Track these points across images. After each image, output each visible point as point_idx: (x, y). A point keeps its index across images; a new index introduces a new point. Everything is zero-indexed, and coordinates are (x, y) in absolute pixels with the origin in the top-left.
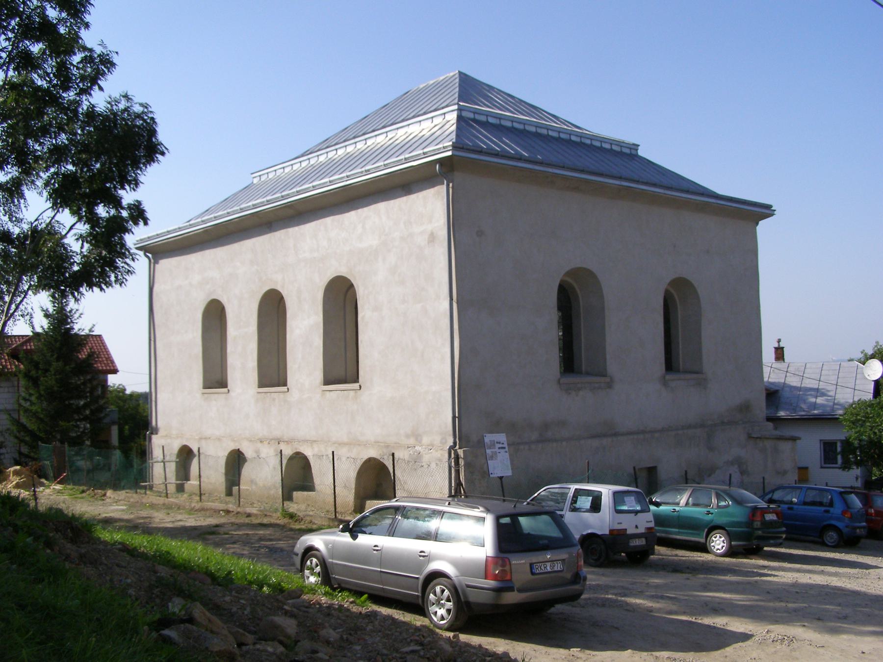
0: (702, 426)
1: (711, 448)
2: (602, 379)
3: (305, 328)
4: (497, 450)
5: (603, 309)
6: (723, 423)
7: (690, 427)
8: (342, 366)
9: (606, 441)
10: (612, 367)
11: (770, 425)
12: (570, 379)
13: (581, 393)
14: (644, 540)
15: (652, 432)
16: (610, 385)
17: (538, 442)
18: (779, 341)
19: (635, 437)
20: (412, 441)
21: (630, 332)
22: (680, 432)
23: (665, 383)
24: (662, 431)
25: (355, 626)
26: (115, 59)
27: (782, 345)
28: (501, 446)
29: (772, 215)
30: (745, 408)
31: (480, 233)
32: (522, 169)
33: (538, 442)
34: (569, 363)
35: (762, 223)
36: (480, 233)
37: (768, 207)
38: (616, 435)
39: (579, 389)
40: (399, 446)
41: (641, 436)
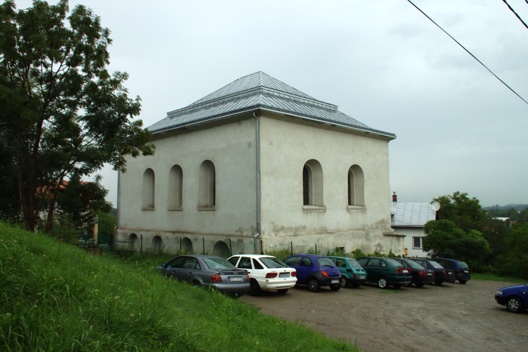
3: (193, 180)
5: (322, 178)
7: (359, 230)
8: (310, 169)
10: (326, 202)
16: (325, 211)
17: (293, 236)
18: (394, 193)
20: (239, 233)
21: (333, 186)
22: (355, 232)
23: (348, 210)
26: (495, 303)
27: (396, 194)
29: (395, 138)
30: (383, 222)
32: (303, 119)
33: (293, 236)
35: (390, 141)
36: (271, 144)
37: (394, 135)
39: (311, 212)
40: (232, 236)
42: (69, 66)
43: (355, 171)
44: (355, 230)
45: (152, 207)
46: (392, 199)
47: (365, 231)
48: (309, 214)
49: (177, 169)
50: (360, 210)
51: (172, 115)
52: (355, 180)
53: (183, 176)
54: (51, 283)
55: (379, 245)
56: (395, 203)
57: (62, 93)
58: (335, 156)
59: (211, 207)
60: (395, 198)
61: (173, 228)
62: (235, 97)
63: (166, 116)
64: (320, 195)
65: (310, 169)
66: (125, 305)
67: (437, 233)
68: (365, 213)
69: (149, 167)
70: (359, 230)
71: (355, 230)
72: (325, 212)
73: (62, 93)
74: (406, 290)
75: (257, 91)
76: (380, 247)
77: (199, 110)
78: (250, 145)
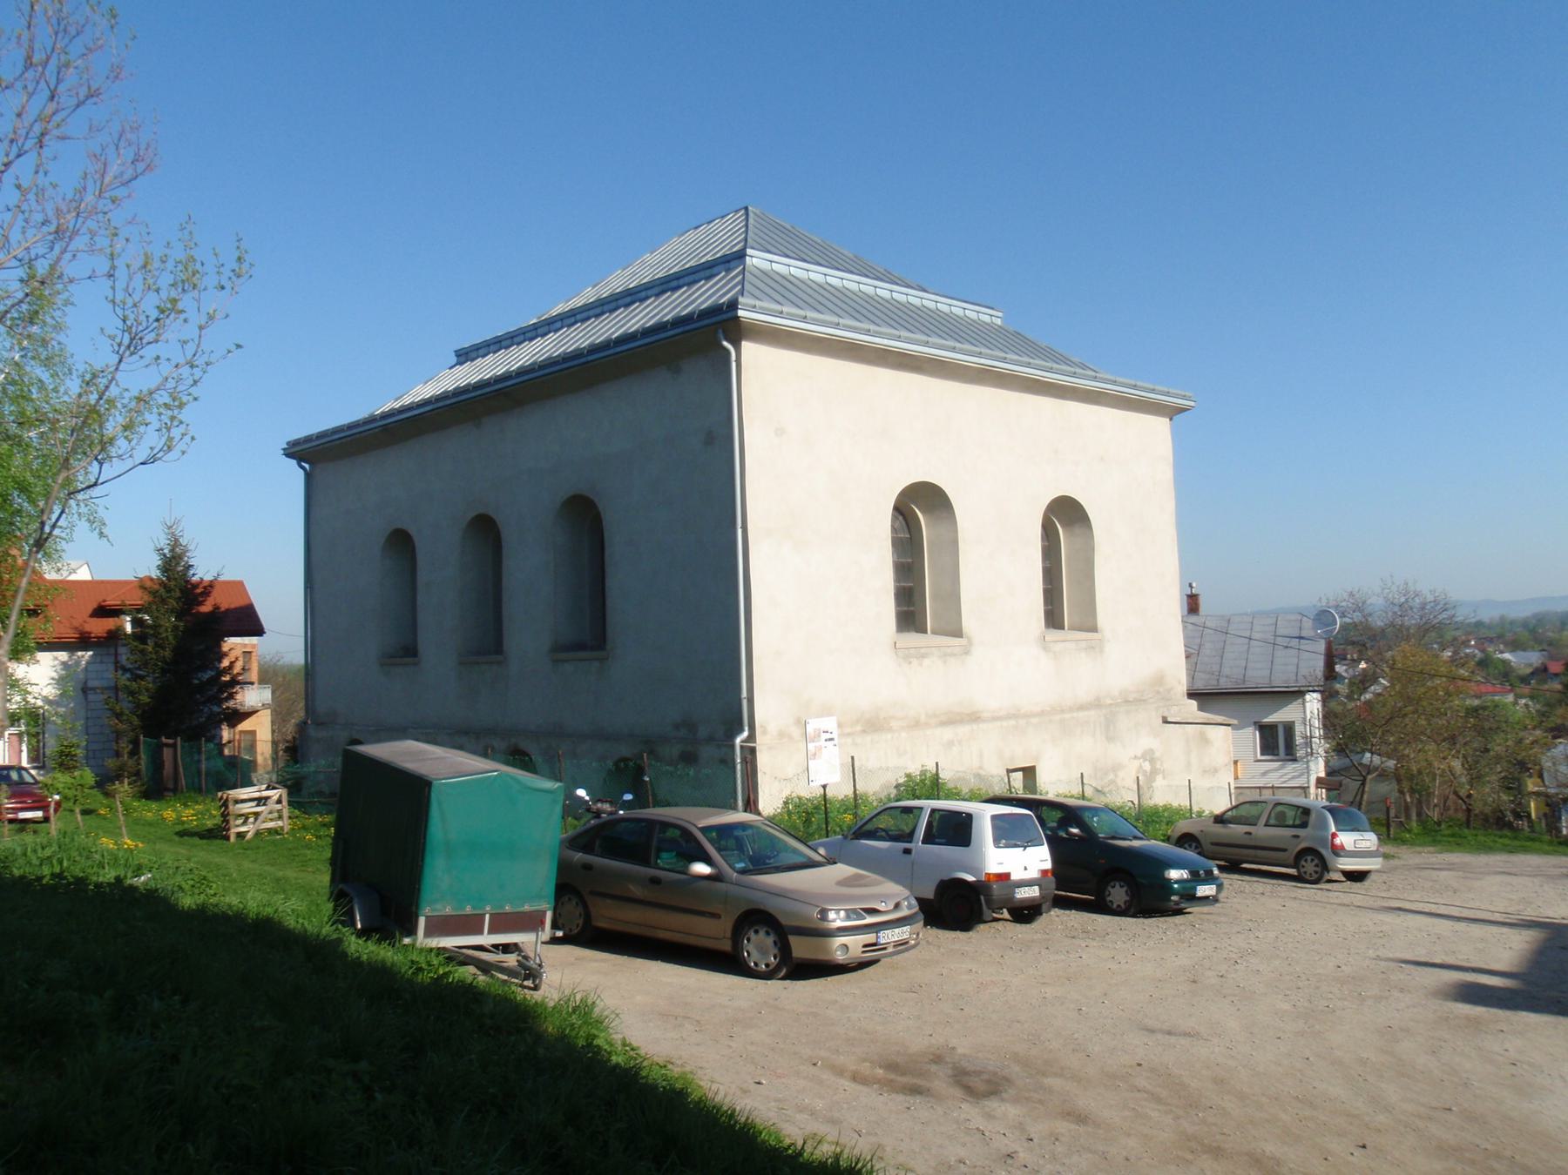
0: (1096, 704)
1: (1110, 739)
2: (957, 641)
3: (533, 567)
4: (822, 743)
6: (1127, 701)
7: (1082, 708)
8: (919, 510)
9: (963, 730)
10: (968, 623)
11: (1194, 703)
12: (912, 639)
13: (926, 662)
14: (1036, 888)
15: (1027, 716)
19: (1005, 724)
21: (995, 564)
22: (1067, 716)
23: (1043, 643)
24: (1042, 713)
25: (728, 762)
28: (828, 736)
30: (1159, 680)
31: (780, 432)
34: (910, 615)
36: (780, 432)
38: (974, 718)
39: (923, 656)
41: (1012, 722)
42: (158, 737)
44: (1071, 710)
45: (407, 652)
47: (1106, 712)
48: (915, 662)
49: (485, 530)
50: (1083, 644)
53: (505, 551)
55: (1149, 756)
57: (249, 836)
59: (593, 649)
64: (952, 598)
65: (919, 510)
66: (93, 234)
68: (1102, 651)
69: (405, 527)
70: (1082, 708)
71: (1071, 710)
72: (967, 653)
73: (249, 836)
76: (1152, 761)
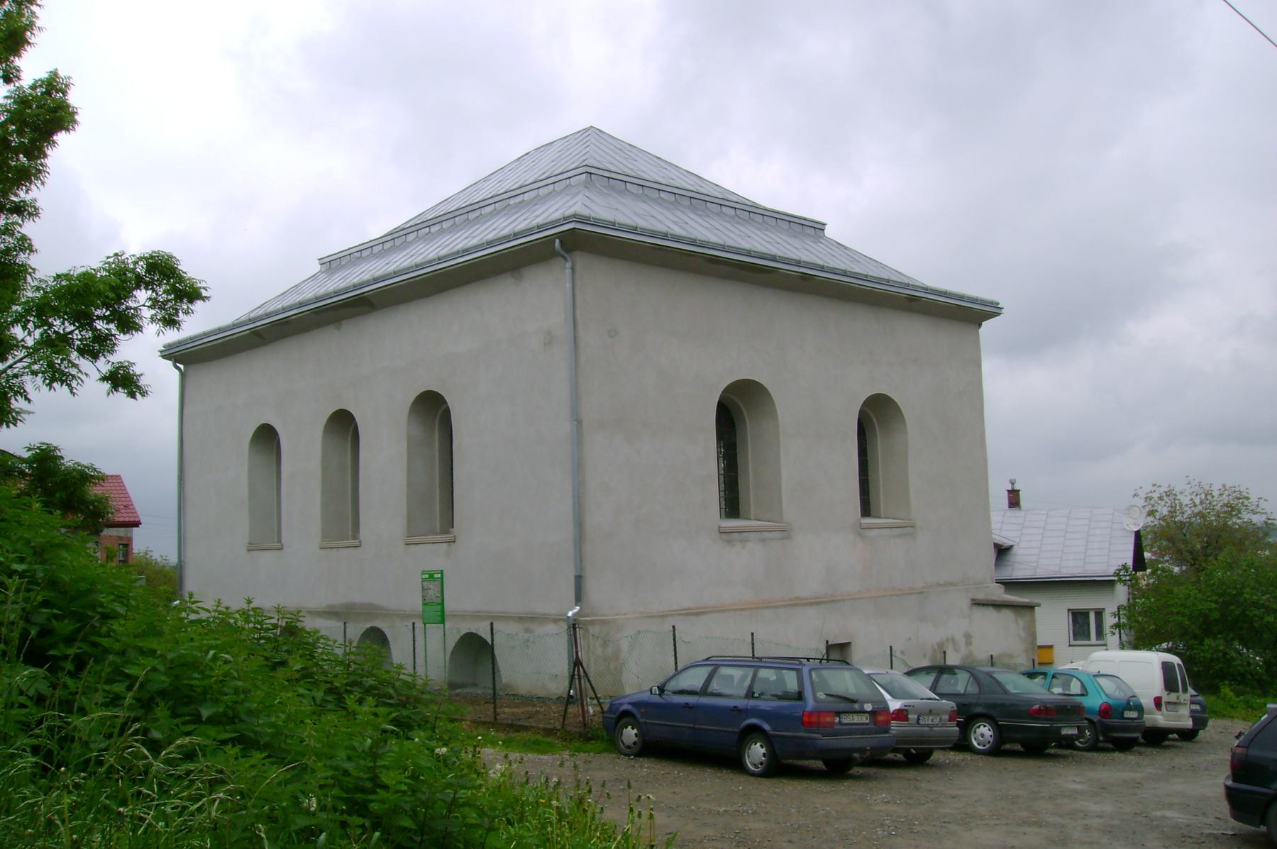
3: (387, 450)
8: (736, 414)
21: (808, 454)
27: (1017, 487)
37: (994, 304)
43: (876, 417)
46: (1005, 501)
49: (343, 424)
51: (331, 264)
52: (880, 444)
54: (142, 652)
56: (1014, 512)
58: (813, 379)
60: (1014, 499)
61: (338, 598)
62: (512, 201)
63: (317, 268)
65: (736, 414)
67: (1238, 694)
74: (1064, 757)
75: (596, 176)
77: (409, 244)
78: (549, 340)
